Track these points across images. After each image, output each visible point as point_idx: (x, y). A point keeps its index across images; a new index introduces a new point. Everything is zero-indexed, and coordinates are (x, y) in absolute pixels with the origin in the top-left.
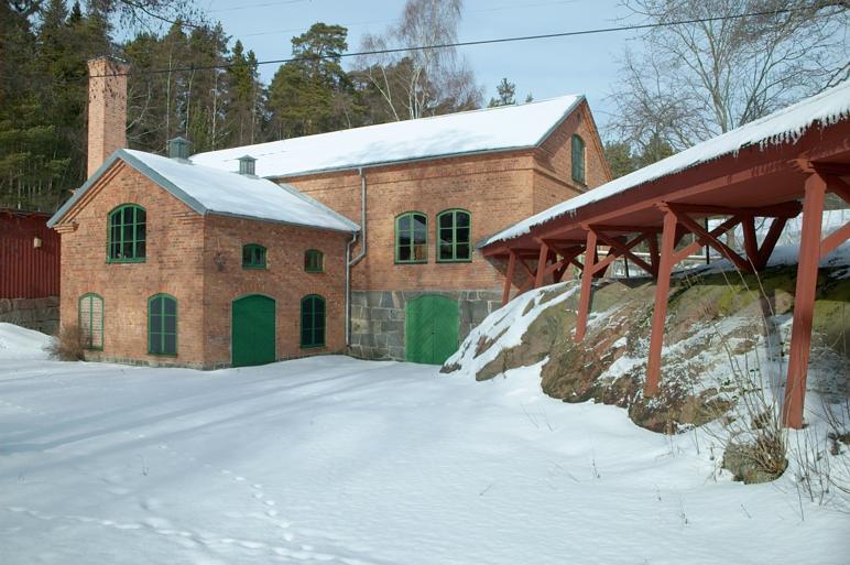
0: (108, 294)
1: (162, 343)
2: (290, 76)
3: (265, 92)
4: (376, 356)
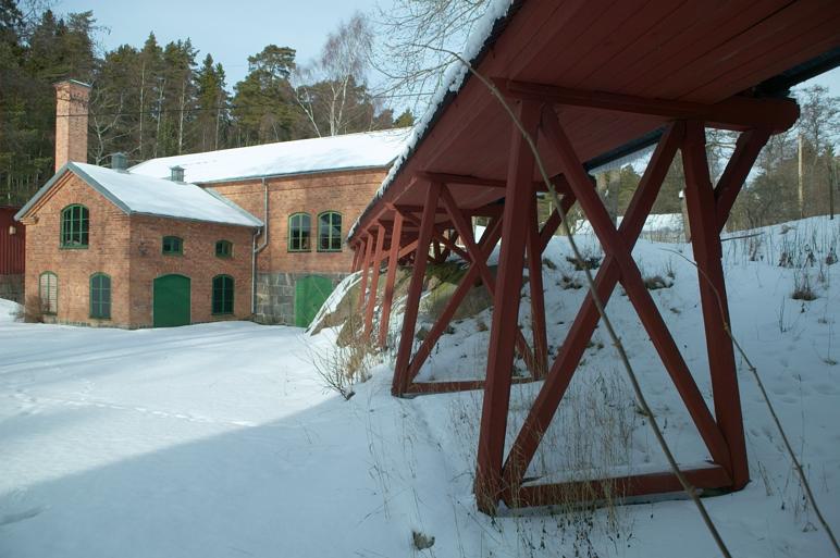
0: (63, 272)
1: (100, 311)
2: (247, 90)
3: (230, 99)
4: (274, 322)
